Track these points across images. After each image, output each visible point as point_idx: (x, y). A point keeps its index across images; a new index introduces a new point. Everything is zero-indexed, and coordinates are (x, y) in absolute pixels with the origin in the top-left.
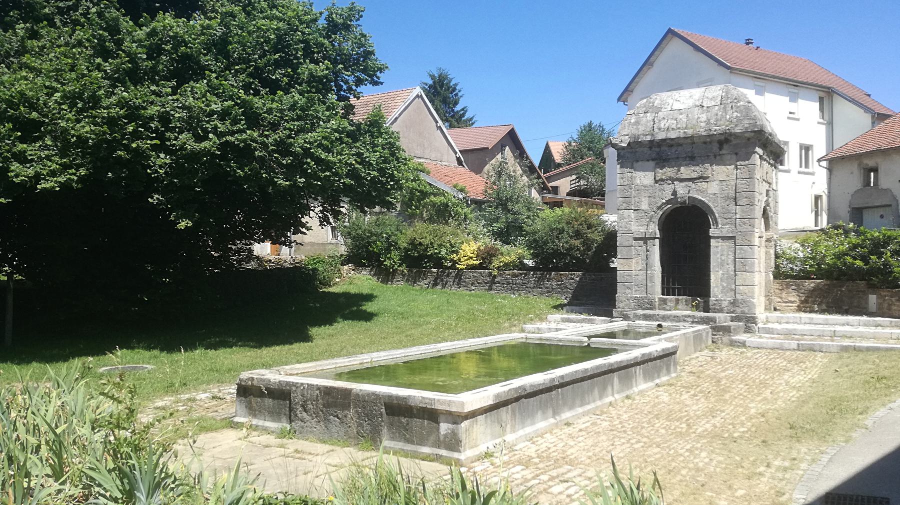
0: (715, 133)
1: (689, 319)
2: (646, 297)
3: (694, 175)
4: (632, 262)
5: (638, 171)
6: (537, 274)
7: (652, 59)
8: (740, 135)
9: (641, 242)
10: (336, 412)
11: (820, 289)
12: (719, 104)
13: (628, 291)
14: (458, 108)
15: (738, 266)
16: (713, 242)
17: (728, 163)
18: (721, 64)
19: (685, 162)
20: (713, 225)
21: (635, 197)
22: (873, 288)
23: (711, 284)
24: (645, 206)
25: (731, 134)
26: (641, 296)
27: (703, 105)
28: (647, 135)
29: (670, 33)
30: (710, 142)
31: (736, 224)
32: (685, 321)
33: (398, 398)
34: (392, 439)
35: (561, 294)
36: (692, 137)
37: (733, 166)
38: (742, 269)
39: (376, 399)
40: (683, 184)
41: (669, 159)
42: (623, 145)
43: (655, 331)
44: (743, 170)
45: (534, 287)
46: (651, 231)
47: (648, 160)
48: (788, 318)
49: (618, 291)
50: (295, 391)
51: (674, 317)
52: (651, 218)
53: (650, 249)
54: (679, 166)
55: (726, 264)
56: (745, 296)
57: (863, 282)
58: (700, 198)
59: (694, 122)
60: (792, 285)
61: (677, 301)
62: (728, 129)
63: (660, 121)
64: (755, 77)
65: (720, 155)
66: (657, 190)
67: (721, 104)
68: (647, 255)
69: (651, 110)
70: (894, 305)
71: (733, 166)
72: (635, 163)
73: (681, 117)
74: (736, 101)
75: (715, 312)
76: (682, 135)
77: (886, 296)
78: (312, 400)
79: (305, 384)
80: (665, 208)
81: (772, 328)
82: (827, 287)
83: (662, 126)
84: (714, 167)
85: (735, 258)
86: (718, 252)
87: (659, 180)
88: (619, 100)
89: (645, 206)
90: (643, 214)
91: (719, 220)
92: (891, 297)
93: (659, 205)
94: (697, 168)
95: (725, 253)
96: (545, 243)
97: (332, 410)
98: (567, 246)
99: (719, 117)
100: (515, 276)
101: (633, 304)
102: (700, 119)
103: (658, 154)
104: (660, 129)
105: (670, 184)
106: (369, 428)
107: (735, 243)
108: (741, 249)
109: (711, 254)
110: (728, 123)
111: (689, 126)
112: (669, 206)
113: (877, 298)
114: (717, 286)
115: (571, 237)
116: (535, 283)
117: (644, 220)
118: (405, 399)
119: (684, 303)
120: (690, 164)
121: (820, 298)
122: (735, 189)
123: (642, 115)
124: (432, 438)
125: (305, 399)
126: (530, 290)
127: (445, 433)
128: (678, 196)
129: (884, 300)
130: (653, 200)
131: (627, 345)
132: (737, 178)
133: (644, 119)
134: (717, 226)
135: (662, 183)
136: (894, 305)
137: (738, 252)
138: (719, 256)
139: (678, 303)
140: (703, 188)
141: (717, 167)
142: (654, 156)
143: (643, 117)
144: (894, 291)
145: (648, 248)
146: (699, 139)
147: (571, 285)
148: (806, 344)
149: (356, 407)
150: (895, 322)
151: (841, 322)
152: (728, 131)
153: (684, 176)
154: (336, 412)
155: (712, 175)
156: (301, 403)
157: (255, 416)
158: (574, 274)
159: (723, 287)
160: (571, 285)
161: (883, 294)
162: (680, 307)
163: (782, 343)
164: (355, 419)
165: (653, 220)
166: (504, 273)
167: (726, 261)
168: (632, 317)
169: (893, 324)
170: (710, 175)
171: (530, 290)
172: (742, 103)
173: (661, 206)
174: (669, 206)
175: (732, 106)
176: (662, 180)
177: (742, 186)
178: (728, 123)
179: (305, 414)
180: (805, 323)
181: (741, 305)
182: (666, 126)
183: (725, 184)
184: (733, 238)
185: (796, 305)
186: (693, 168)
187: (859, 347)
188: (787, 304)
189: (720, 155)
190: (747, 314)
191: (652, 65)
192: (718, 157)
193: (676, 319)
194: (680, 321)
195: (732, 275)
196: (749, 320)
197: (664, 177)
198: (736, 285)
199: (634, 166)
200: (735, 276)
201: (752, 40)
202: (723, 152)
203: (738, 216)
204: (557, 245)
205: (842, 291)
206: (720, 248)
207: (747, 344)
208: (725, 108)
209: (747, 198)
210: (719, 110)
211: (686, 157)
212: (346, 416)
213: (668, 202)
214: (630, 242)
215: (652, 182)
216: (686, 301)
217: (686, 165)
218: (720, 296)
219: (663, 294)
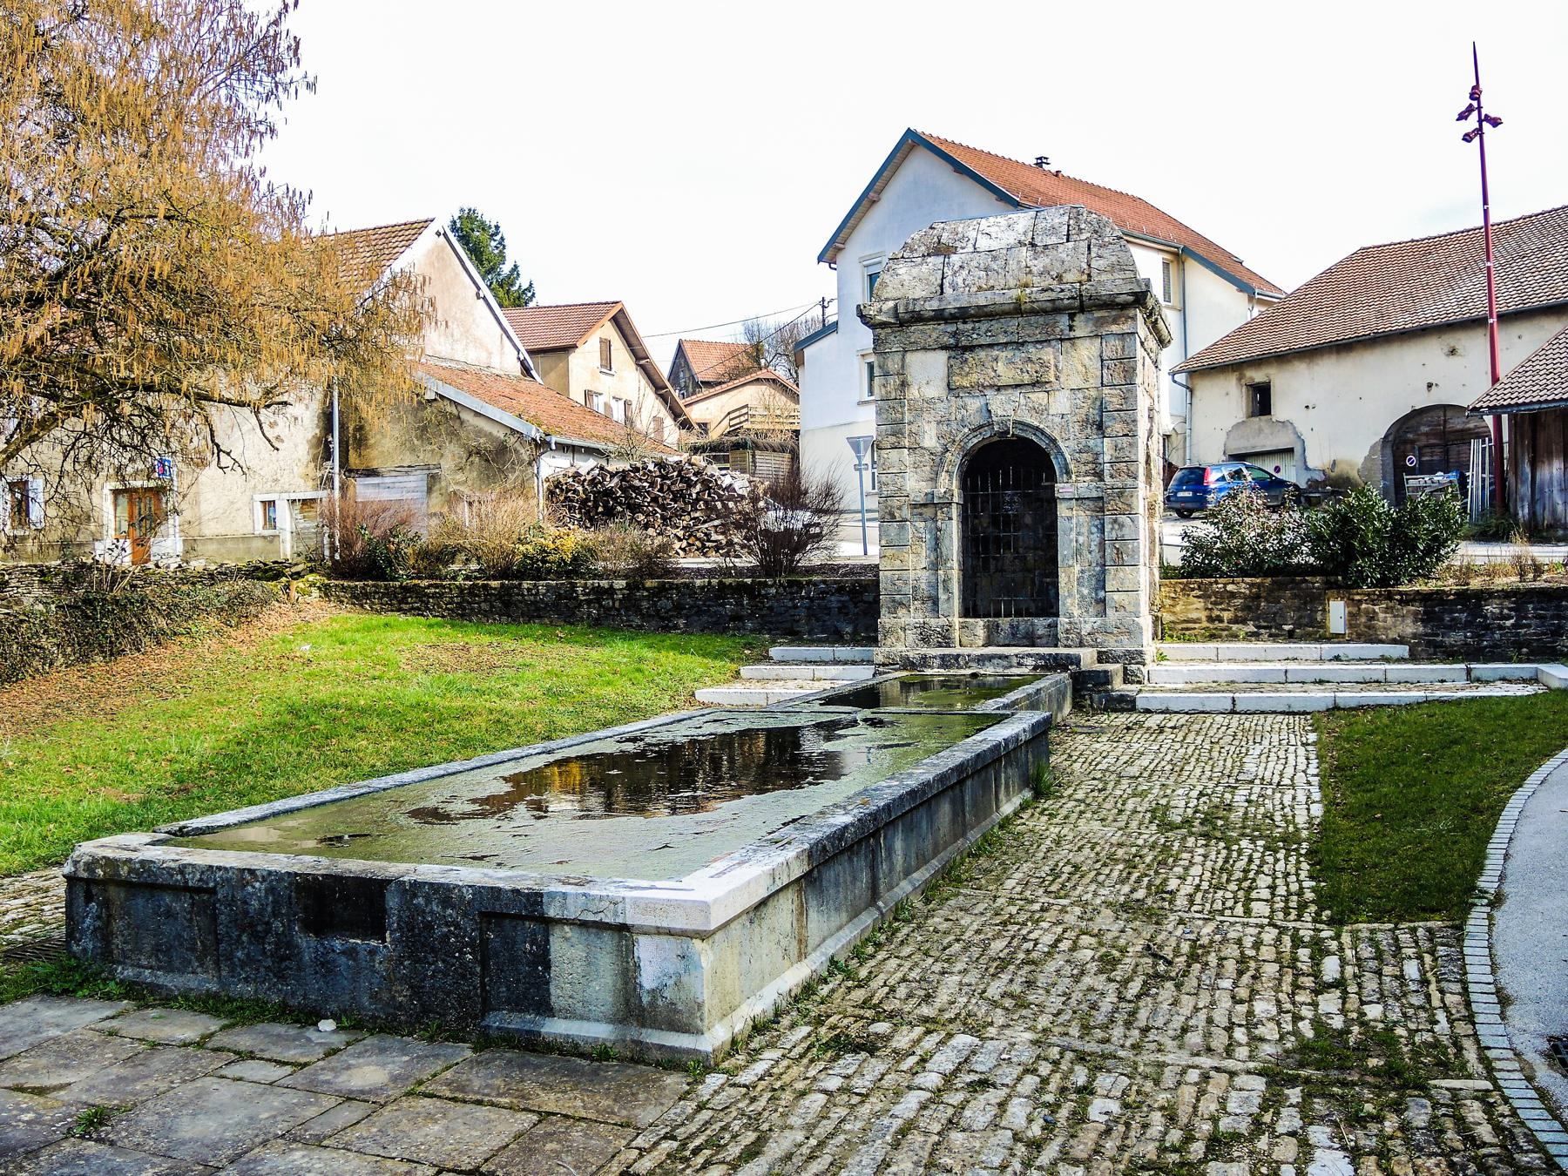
14: (506, 269)
16: (1062, 510)
21: (910, 423)
29: (912, 142)
53: (944, 527)
83: (959, 280)
88: (820, 259)
138: (1073, 535)
159: (1083, 597)
170: (1053, 379)
177: (1112, 398)
183: (1080, 395)
207: (1140, 705)
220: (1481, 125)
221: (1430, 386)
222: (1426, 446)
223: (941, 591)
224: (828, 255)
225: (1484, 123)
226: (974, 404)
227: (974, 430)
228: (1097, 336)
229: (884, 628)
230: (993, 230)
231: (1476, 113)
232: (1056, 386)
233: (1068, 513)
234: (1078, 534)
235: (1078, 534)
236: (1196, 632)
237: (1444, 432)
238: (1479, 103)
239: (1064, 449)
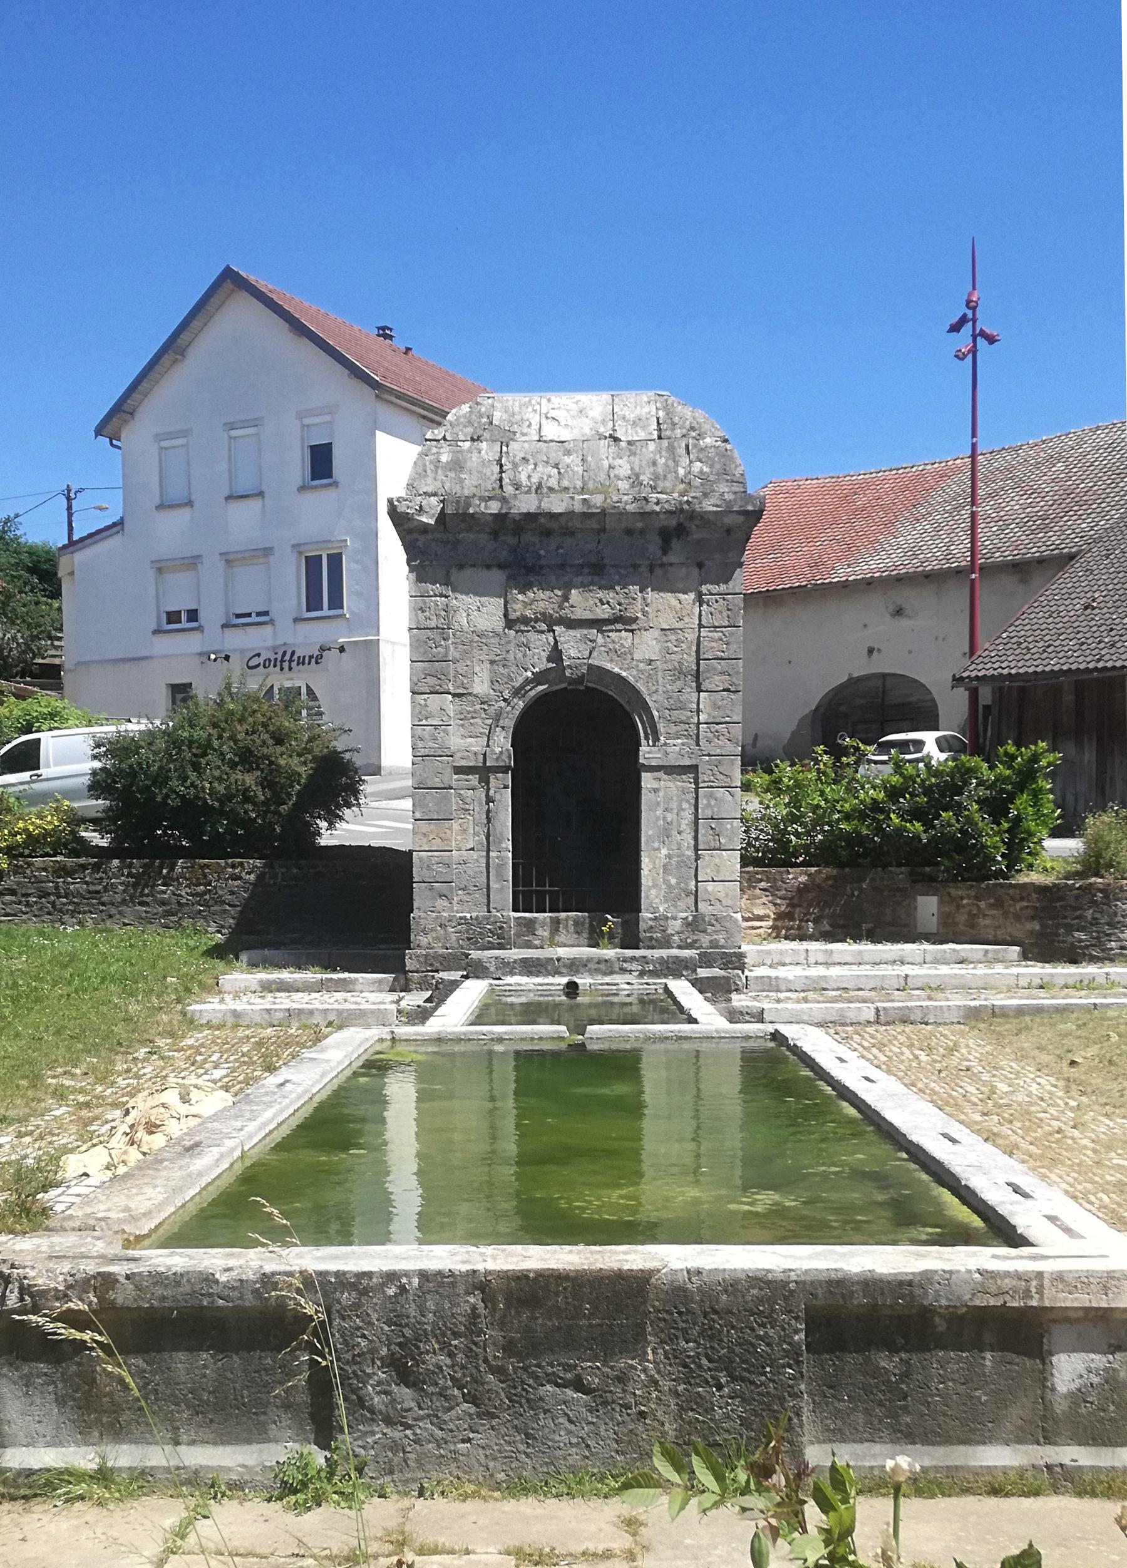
0: (657, 508)
1: (635, 966)
2: (488, 918)
3: (604, 612)
4: (450, 828)
5: (462, 593)
6: (130, 866)
7: (184, 338)
8: (712, 518)
9: (474, 779)
10: (569, 1368)
11: (819, 886)
12: (656, 437)
13: (441, 903)
15: (704, 835)
16: (647, 780)
17: (681, 586)
18: (357, 373)
19: (580, 579)
20: (647, 738)
22: (928, 883)
23: (644, 880)
24: (481, 686)
25: (693, 515)
26: (474, 915)
27: (618, 435)
28: (490, 498)
30: (642, 532)
31: (698, 735)
32: (623, 970)
33: (871, 1284)
34: (835, 1435)
35: (204, 918)
36: (603, 513)
37: (692, 596)
38: (712, 844)
39: (771, 1301)
40: (578, 633)
41: (541, 567)
42: (424, 519)
43: (557, 999)
44: (716, 605)
45: (124, 902)
46: (498, 750)
47: (488, 567)
48: (781, 952)
49: (415, 905)
50: (357, 1306)
51: (598, 963)
52: (497, 717)
54: (567, 587)
55: (674, 832)
56: (718, 906)
57: (903, 869)
58: (616, 670)
59: (602, 477)
60: (761, 880)
61: (556, 925)
62: (688, 502)
63: (515, 466)
64: (424, 417)
65: (661, 565)
66: (512, 647)
67: (660, 437)
68: (488, 812)
69: (486, 435)
70: (985, 915)
71: (692, 596)
72: (453, 571)
73: (567, 460)
74: (694, 434)
75: (653, 948)
76: (578, 508)
77: (962, 898)
78: (443, 1336)
79: (406, 1274)
80: (532, 693)
81: (777, 978)
82: (830, 882)
83: (523, 478)
84: (651, 595)
85: (697, 818)
86: (658, 804)
87: (516, 621)
88: (98, 432)
89: (481, 686)
90: (478, 707)
91: (661, 727)
92: (977, 898)
93: (517, 685)
94: (610, 596)
95: (674, 805)
96: (161, 778)
97: (548, 1364)
98: (221, 788)
99: (660, 470)
100: (62, 871)
101: (454, 937)
102: (616, 472)
103: (514, 551)
104: (517, 486)
105: (542, 632)
106: (738, 1408)
107: (696, 783)
108: (711, 795)
109: (643, 807)
110: (682, 486)
111: (591, 485)
112: (541, 688)
113: (941, 902)
114: (655, 886)
115: (233, 765)
116: (124, 891)
117: (478, 720)
118: (903, 1286)
119: (572, 929)
120: (592, 583)
121: (818, 905)
122: (698, 651)
123: (468, 444)
124: (1017, 1412)
125: (408, 1332)
126: (113, 911)
127: (1073, 1387)
128: (565, 664)
129: (958, 907)
130: (501, 669)
131: (686, 1038)
132: (700, 626)
133: (475, 457)
134: (656, 739)
135: (523, 628)
136: (985, 915)
137: (702, 802)
139: (557, 930)
140: (622, 646)
141: (655, 595)
142: (504, 555)
143: (470, 451)
144: (983, 886)
145: (492, 792)
146: (620, 521)
147: (232, 893)
148: (894, 1008)
149: (672, 1339)
150: (994, 951)
151: (890, 957)
152: (686, 507)
153: (579, 614)
154: (569, 1368)
155: (645, 614)
156: (384, 1351)
157: (117, 1432)
158: (241, 864)
159: (670, 887)
160: (232, 893)
161: (953, 892)
162: (561, 938)
163: (842, 1009)
164: (666, 1385)
165: (501, 723)
166: (29, 864)
167: (675, 824)
168: (492, 969)
169: (990, 955)
170: (639, 615)
171: (113, 911)
172: (708, 440)
173: (522, 687)
174: (541, 688)
175: (687, 447)
176: (525, 620)
178: (682, 486)
179: (405, 1395)
180: (816, 963)
181: (710, 929)
182: (535, 480)
183: (673, 637)
184: (693, 769)
185: (770, 923)
186: (600, 595)
187: (1002, 1007)
188: (750, 924)
189: (661, 565)
190: (723, 947)
191: (182, 353)
192: (659, 572)
193: (602, 967)
194: (612, 973)
195: (689, 857)
196: (729, 962)
197: (529, 613)
198: (697, 882)
199: (452, 579)
200: (696, 861)
201: (391, 330)
202: (672, 558)
203: (703, 717)
204: (196, 787)
205: (860, 889)
206: (661, 794)
208: (671, 449)
209: (723, 673)
210: (659, 451)
211: (582, 566)
212: (622, 1379)
213: (538, 678)
214: (446, 779)
215: (499, 624)
216: (577, 923)
217: (584, 586)
218: (661, 909)
219: (515, 910)
220: (974, 341)
221: (871, 651)
224: (109, 429)
225: (979, 338)
226: (539, 645)
230: (561, 415)
231: (970, 324)
232: (642, 622)
233: (655, 785)
234: (666, 810)
235: (666, 810)
236: (761, 931)
238: (974, 314)
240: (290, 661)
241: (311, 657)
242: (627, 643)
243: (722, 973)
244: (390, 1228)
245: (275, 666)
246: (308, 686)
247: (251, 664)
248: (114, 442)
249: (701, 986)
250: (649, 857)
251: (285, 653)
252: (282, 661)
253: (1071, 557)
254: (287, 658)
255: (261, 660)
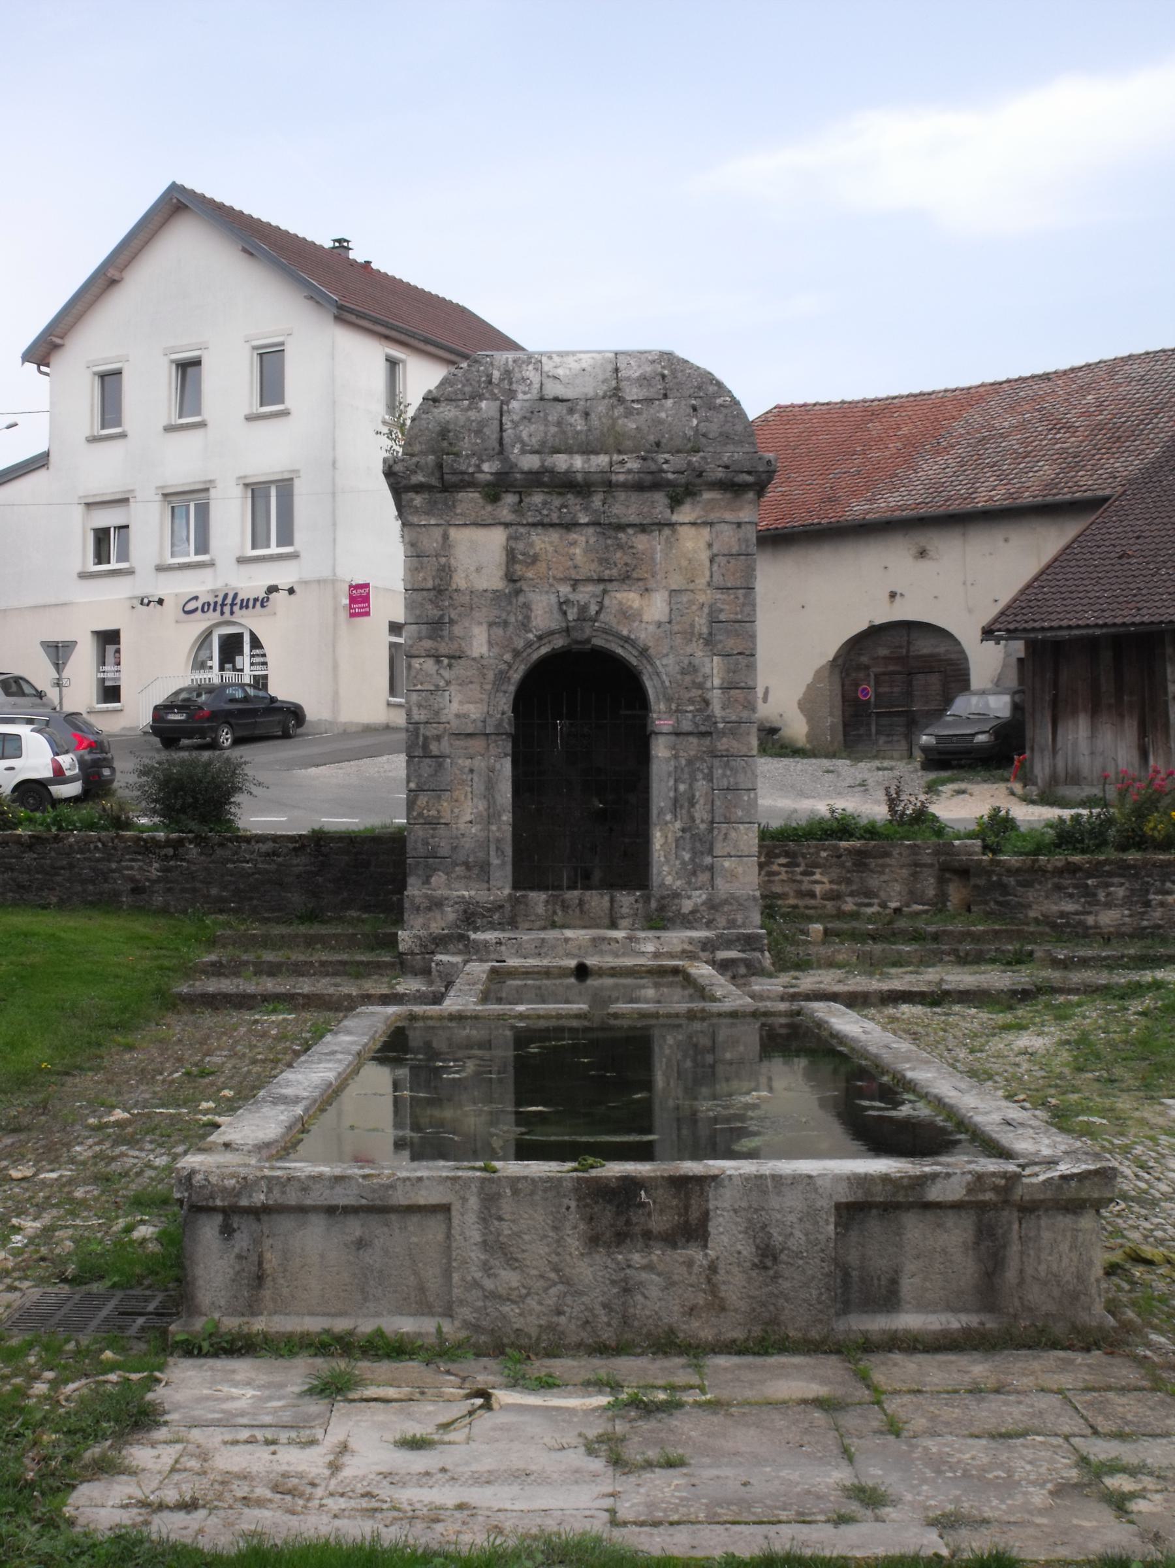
88: (28, 357)
159: (684, 863)
201: (348, 242)
221: (893, 595)
222: (884, 674)
223: (492, 853)
227: (540, 638)
228: (705, 524)
229: (413, 903)
237: (907, 657)
239: (661, 669)
240: (232, 605)
241: (256, 600)
242: (636, 605)
243: (741, 955)
244: (158, 1394)
245: (215, 610)
246: (252, 634)
247: (188, 608)
248: (43, 368)
249: (723, 966)
250: (661, 830)
251: (226, 596)
252: (223, 605)
253: (1105, 499)
254: (229, 601)
255: (199, 604)
